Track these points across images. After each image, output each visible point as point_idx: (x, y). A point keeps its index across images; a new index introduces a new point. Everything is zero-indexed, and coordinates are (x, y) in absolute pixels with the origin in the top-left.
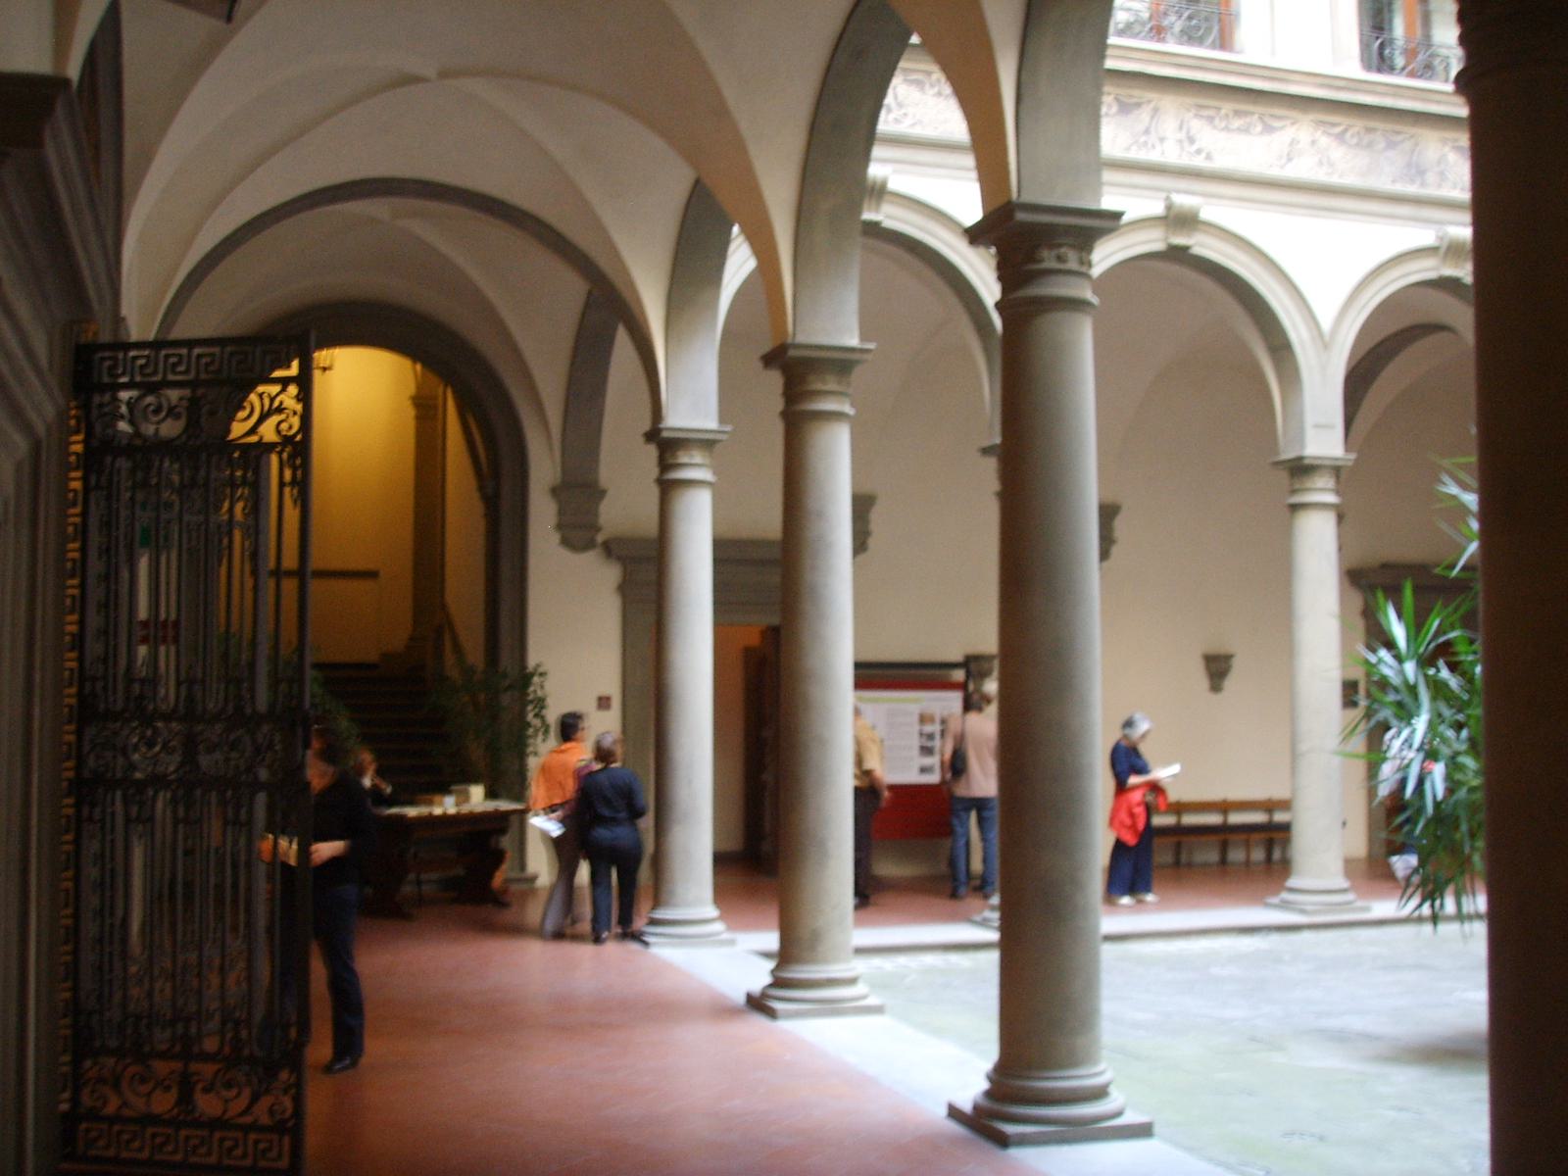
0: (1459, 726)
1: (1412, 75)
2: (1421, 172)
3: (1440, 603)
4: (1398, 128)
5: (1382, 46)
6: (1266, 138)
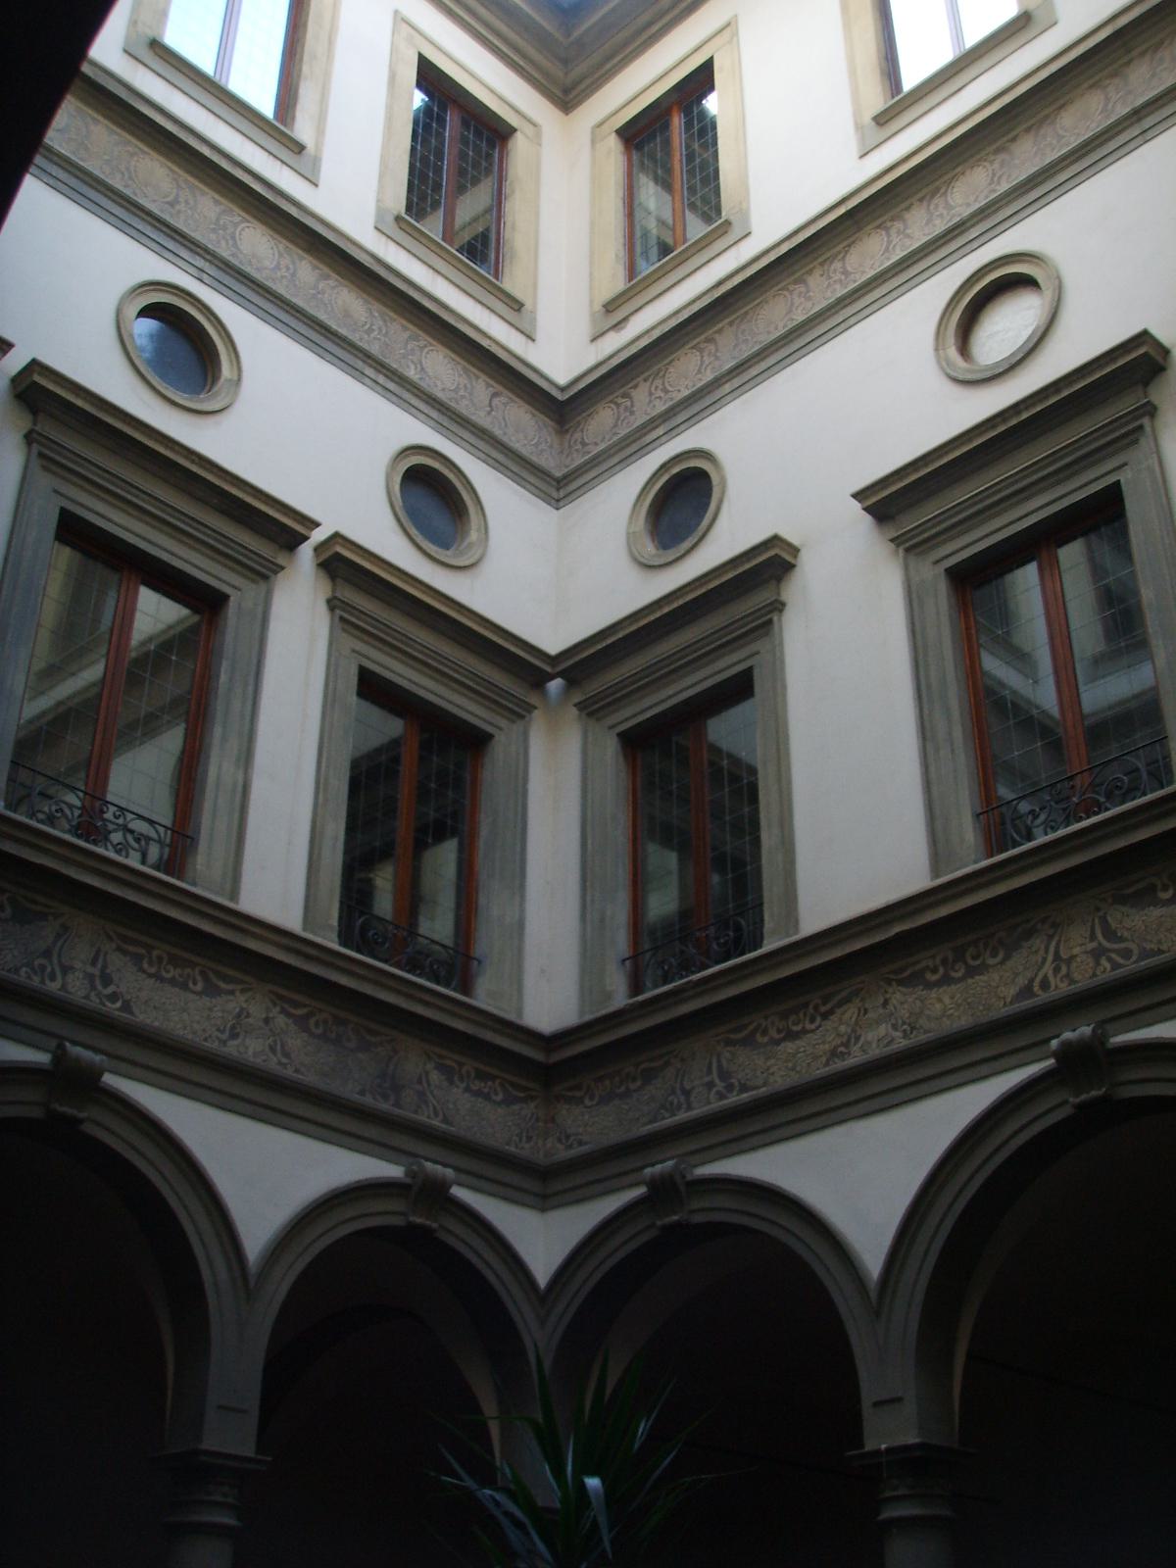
6: (206, 1001)
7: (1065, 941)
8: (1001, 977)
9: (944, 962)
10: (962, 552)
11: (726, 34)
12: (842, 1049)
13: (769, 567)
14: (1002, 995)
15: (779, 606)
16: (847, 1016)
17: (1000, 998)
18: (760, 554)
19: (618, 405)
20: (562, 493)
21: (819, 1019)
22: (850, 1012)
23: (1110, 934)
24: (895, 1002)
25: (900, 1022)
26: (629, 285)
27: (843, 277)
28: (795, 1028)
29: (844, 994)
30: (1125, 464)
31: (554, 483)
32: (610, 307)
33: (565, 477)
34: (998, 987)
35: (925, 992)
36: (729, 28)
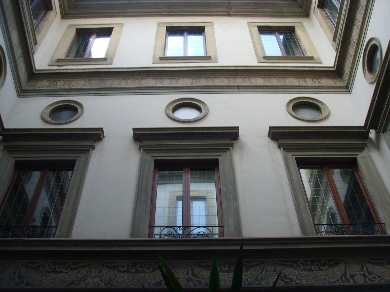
7: (177, 272)
8: (149, 277)
9: (128, 265)
10: (159, 157)
11: (120, 25)
12: (77, 282)
13: (95, 136)
14: (149, 282)
15: (93, 148)
16: (82, 272)
17: (148, 283)
18: (95, 131)
19: (51, 82)
20: (22, 94)
21: (69, 270)
22: (84, 271)
23: (194, 274)
24: (104, 273)
25: (104, 280)
26: (65, 58)
27: (139, 84)
28: (58, 270)
29: (83, 264)
30: (221, 156)
31: (21, 90)
32: (58, 61)
33: (25, 90)
34: (147, 279)
35: (117, 273)
36: (121, 25)
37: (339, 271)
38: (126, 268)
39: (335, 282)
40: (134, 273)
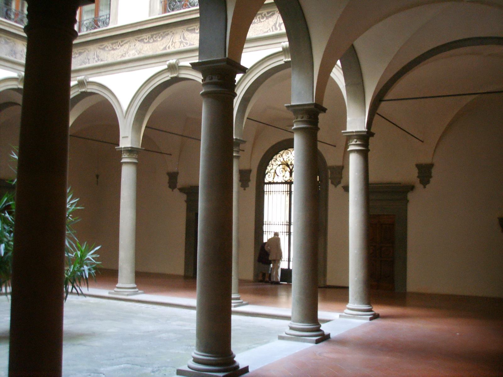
0: (10, 232)
1: (16, 22)
2: (15, 53)
3: (7, 193)
4: (102, 44)
5: (7, 10)
23: (184, 38)
37: (272, 21)
38: (148, 39)
39: (267, 32)
40: (152, 42)
